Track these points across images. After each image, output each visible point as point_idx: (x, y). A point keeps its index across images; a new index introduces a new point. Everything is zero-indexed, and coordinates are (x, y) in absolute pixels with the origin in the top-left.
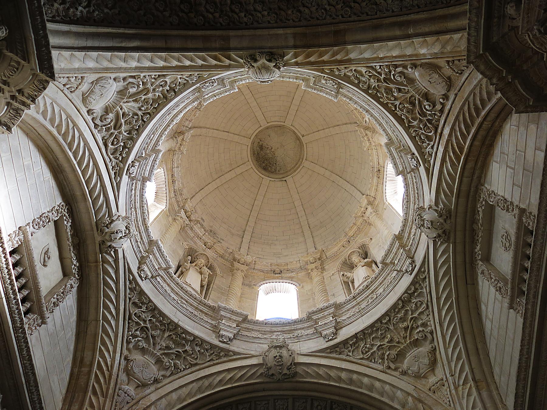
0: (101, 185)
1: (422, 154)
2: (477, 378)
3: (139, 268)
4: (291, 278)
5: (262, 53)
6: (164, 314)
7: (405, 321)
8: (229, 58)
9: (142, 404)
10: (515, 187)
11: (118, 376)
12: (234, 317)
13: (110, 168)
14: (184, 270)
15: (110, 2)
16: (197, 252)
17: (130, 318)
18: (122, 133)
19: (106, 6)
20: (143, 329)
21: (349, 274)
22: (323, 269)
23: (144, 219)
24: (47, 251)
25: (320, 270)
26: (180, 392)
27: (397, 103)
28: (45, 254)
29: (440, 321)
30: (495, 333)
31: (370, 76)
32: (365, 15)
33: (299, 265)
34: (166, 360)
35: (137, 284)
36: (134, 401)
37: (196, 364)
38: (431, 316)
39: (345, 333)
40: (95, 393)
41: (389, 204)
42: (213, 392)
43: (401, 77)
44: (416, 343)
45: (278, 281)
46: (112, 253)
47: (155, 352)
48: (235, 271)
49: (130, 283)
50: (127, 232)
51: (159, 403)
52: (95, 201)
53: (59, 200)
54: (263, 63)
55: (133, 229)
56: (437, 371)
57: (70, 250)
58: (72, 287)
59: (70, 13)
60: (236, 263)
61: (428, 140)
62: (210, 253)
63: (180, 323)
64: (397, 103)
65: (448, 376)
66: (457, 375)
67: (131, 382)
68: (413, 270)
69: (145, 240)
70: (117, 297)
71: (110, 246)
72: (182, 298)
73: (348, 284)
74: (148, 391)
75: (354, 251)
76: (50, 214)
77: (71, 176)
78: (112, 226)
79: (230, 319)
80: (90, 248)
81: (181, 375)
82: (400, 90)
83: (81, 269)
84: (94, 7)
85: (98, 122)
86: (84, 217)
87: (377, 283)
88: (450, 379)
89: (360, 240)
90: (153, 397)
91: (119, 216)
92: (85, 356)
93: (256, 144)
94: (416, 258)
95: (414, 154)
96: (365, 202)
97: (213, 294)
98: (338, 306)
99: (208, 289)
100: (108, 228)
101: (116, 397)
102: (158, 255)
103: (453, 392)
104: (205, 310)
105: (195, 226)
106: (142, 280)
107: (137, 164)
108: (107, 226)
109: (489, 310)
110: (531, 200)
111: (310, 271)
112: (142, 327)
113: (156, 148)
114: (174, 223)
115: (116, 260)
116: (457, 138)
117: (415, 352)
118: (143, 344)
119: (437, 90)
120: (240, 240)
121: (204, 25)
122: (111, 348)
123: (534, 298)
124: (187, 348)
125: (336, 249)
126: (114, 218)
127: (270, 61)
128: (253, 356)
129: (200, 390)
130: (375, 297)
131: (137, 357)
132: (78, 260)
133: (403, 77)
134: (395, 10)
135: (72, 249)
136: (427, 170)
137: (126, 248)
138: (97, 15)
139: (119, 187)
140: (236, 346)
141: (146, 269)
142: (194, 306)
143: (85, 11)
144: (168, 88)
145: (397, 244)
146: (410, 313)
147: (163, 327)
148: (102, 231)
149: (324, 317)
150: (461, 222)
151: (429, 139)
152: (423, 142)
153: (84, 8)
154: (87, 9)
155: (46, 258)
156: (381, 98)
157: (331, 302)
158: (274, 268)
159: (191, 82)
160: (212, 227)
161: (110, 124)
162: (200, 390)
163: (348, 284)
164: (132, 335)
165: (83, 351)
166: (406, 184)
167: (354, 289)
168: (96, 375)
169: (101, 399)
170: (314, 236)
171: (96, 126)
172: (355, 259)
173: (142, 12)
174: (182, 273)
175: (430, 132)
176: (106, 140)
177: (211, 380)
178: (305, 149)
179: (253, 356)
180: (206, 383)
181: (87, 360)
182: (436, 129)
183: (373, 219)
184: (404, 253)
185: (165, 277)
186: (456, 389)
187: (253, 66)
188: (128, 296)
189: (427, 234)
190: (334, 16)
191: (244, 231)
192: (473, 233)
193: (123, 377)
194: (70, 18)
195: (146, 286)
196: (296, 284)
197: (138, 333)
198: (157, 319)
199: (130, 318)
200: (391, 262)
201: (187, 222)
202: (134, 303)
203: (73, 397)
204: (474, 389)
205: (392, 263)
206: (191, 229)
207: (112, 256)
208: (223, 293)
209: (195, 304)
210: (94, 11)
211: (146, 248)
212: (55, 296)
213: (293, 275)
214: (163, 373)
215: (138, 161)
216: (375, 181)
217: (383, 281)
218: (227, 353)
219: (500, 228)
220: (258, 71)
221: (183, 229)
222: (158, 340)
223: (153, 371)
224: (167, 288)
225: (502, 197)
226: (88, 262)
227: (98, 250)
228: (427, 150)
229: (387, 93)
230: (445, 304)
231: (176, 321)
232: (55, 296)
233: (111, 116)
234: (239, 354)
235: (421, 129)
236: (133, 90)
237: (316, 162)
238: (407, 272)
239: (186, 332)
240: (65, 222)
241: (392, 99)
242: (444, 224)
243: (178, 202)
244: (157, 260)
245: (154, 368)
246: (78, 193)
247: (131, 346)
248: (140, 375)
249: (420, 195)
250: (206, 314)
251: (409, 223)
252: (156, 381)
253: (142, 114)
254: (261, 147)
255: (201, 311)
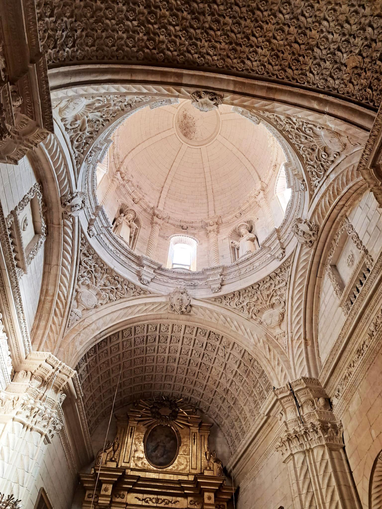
0: (65, 164)
1: (310, 185)
2: (307, 338)
3: (88, 228)
4: (194, 234)
5: (206, 93)
6: (105, 262)
7: (268, 290)
8: (179, 91)
9: (87, 322)
10: (367, 234)
11: (71, 302)
12: (152, 266)
13: (74, 158)
14: (118, 224)
15: (90, 41)
16: (128, 207)
17: (80, 264)
18: (85, 134)
19: (87, 45)
20: (89, 272)
21: (236, 243)
22: (218, 232)
23: (94, 190)
24: (25, 220)
25: (216, 233)
26: (112, 315)
27: (302, 146)
28: (24, 222)
29: (293, 295)
30: (326, 314)
31: (287, 123)
32: (295, 81)
33: (201, 224)
34: (104, 293)
35: (87, 241)
36: (81, 320)
37: (123, 298)
38: (287, 291)
39: (227, 289)
40: (56, 314)
41: (277, 196)
42: (134, 317)
43: (310, 131)
44: (273, 306)
45: (184, 235)
46: (71, 219)
47: (97, 288)
48: (154, 224)
49: (82, 239)
50: (83, 206)
51: (97, 322)
52: (61, 183)
53: (34, 181)
54: (206, 100)
55: (87, 202)
56: (282, 324)
57: (41, 216)
58: (41, 243)
59: (59, 55)
60: (155, 217)
61: (318, 177)
62: (136, 208)
63: (116, 269)
64: (302, 146)
65: (289, 331)
66: (295, 333)
67: (80, 307)
68: (282, 258)
69: (93, 206)
70: (73, 250)
71: (70, 215)
72: (117, 248)
73: (235, 250)
74: (91, 313)
75: (243, 225)
76: (29, 195)
77: (45, 166)
78: (73, 201)
79: (149, 266)
80: (55, 215)
81: (113, 304)
82: (306, 138)
83: (47, 229)
84: (77, 46)
85: (69, 126)
86: (52, 193)
87: (255, 258)
88: (290, 334)
89: (249, 217)
90: (94, 318)
91: (77, 193)
92: (49, 289)
93: (181, 112)
94: (287, 250)
95: (304, 181)
96: (259, 187)
97: (138, 244)
98: (224, 268)
99: (134, 239)
100: (69, 203)
101: (69, 316)
102: (102, 217)
103: (290, 342)
104: (133, 258)
105: (126, 185)
106: (90, 237)
107: (94, 154)
108: (69, 202)
109: (326, 298)
110: (374, 248)
111: (208, 232)
112: (88, 271)
113: (108, 139)
114: (112, 184)
115: (73, 225)
116: (338, 184)
117: (271, 311)
118: (88, 282)
119: (334, 148)
120: (159, 195)
121: (164, 61)
122: (67, 285)
123: (355, 314)
124: (119, 286)
125: (230, 217)
126: (74, 195)
127: (212, 100)
128: (163, 296)
129: (125, 315)
130: (252, 269)
131: (83, 289)
132: (46, 223)
133: (311, 131)
134: (319, 87)
135: (42, 216)
136: (311, 196)
137: (81, 217)
138: (80, 53)
139: (79, 172)
140: (152, 287)
141: (93, 229)
142: (125, 255)
143: (70, 51)
144: (126, 103)
145: (276, 235)
146: (274, 286)
147: (103, 271)
148: (65, 205)
149: (214, 274)
150: (323, 237)
151: (318, 176)
152: (313, 177)
153: (70, 48)
154: (72, 49)
155: (25, 225)
156: (291, 139)
157: (221, 264)
158: (182, 224)
159: (145, 101)
160: (138, 182)
161: (77, 127)
162: (125, 315)
163: (235, 250)
164: (81, 276)
165: (47, 285)
166: (293, 196)
167: (238, 258)
168: (57, 303)
169: (60, 319)
170: (215, 199)
171: (67, 129)
172: (243, 231)
173: (115, 48)
174: (117, 226)
175: (320, 172)
176: (73, 138)
177: (133, 309)
178: (221, 125)
179: (163, 296)
180: (130, 311)
181: (50, 292)
182: (325, 171)
183: (262, 203)
184: (279, 244)
185: (106, 233)
186: (292, 341)
187: (198, 101)
188: (80, 248)
189: (298, 239)
190: (270, 74)
191: (163, 187)
192: (330, 247)
193: (74, 303)
194: (59, 59)
195: (93, 242)
196: (197, 240)
197: (86, 274)
198: (99, 266)
199: (80, 264)
200: (268, 247)
201: (122, 182)
202: (84, 254)
203: (41, 316)
204: (303, 345)
205: (269, 247)
206: (124, 186)
207: (70, 222)
208: (144, 243)
209: (126, 254)
210: (77, 51)
211: (93, 211)
212: (31, 252)
213: (195, 232)
214: (100, 301)
215: (95, 152)
216: (270, 172)
217: (259, 258)
218: (145, 292)
219: (350, 249)
220: (200, 105)
221: (118, 188)
222: (99, 280)
223: (94, 300)
224: (107, 241)
225: (357, 233)
226: (53, 224)
227: (61, 217)
228: (315, 182)
229: (296, 138)
230: (298, 286)
231: (112, 267)
232: (31, 252)
233: (79, 122)
234: (154, 293)
235: (314, 168)
236: (97, 105)
237: (227, 138)
238: (278, 258)
239: (118, 275)
240: (38, 197)
241: (300, 142)
242: (312, 236)
243: (115, 164)
244: (101, 221)
245: (95, 298)
246: (49, 176)
247: (80, 283)
248: (86, 302)
249: (300, 208)
250: (133, 261)
251: (288, 223)
252: (96, 307)
253: (103, 121)
254: (185, 116)
255: (130, 259)
